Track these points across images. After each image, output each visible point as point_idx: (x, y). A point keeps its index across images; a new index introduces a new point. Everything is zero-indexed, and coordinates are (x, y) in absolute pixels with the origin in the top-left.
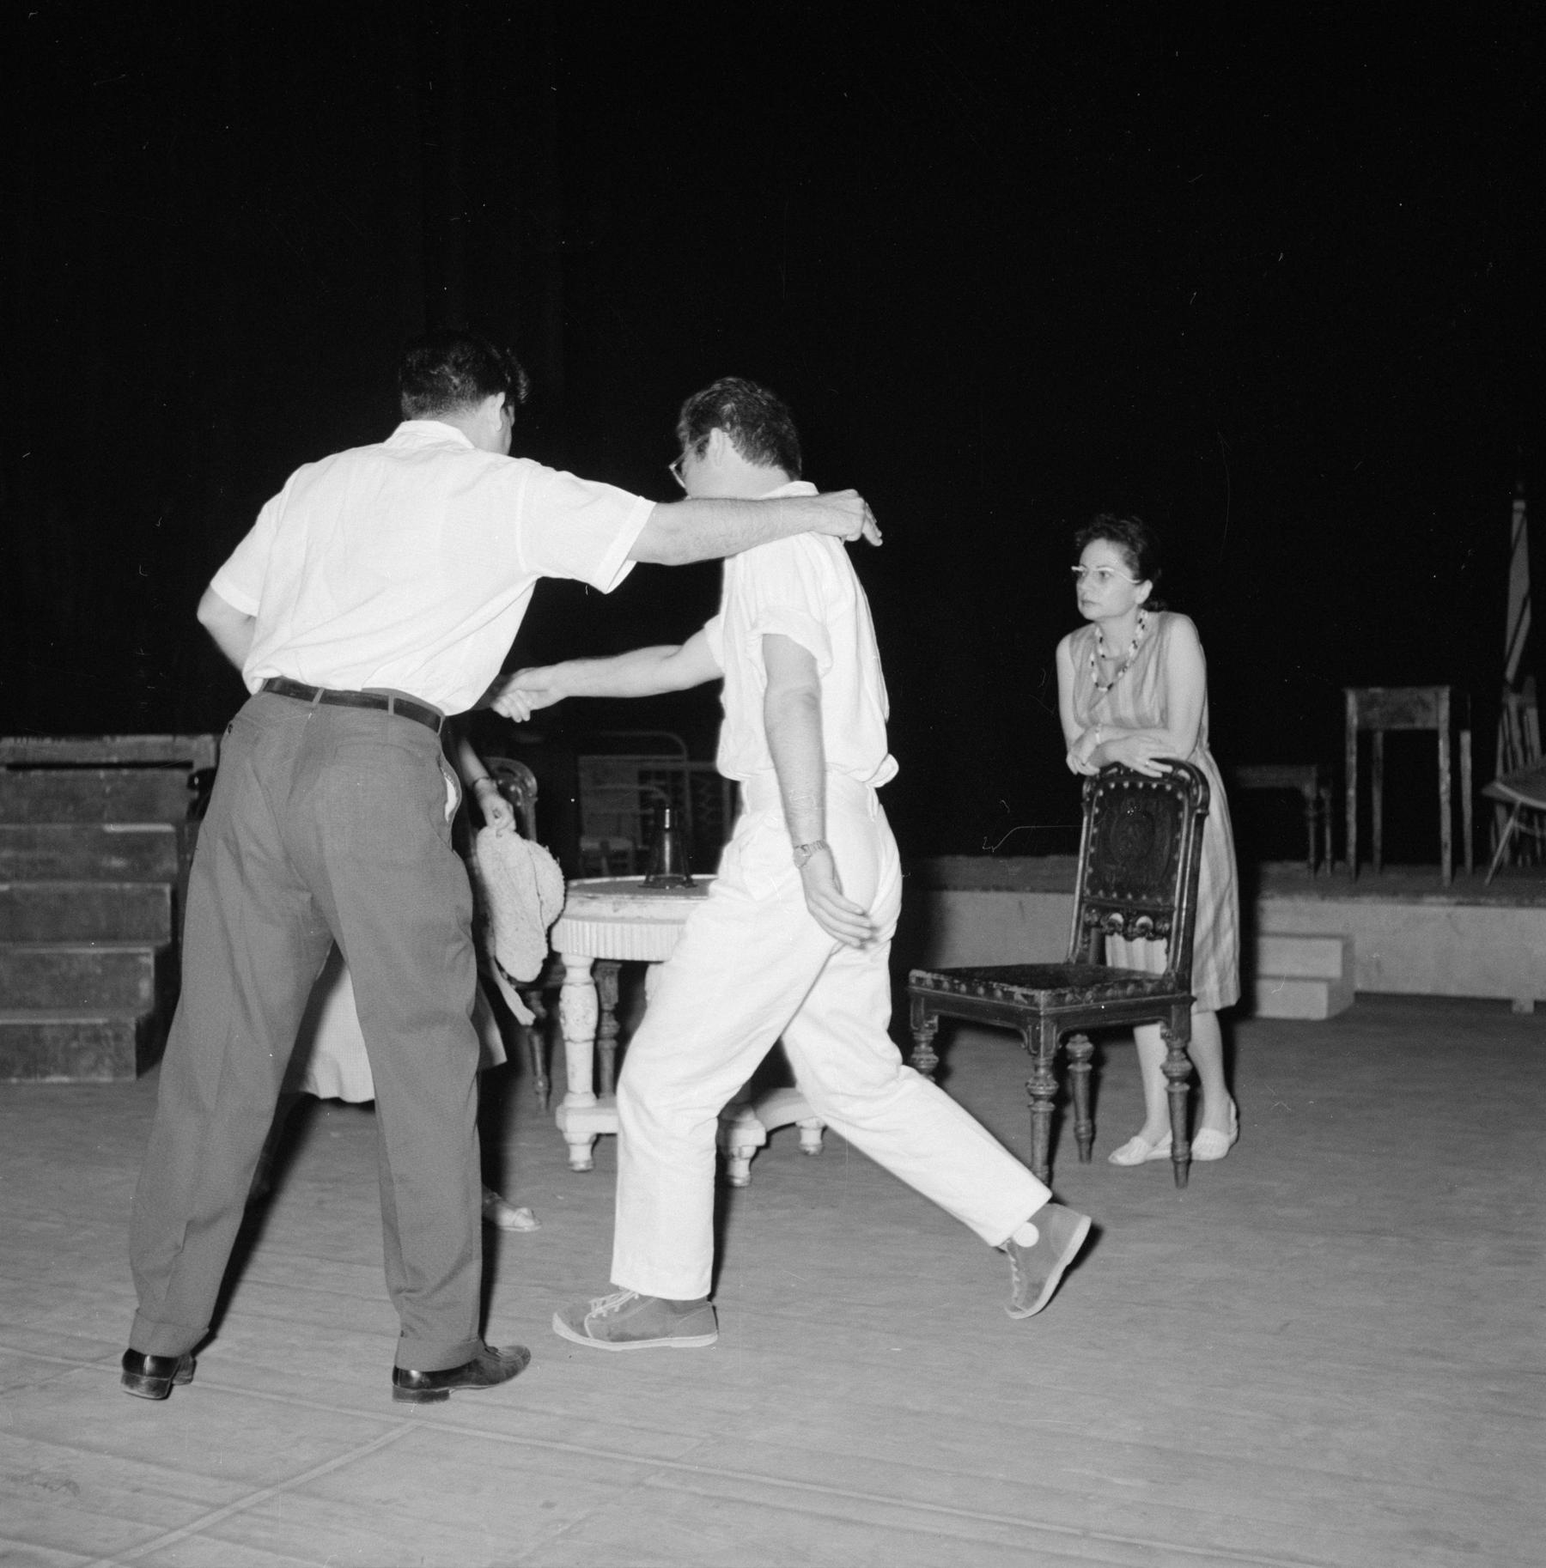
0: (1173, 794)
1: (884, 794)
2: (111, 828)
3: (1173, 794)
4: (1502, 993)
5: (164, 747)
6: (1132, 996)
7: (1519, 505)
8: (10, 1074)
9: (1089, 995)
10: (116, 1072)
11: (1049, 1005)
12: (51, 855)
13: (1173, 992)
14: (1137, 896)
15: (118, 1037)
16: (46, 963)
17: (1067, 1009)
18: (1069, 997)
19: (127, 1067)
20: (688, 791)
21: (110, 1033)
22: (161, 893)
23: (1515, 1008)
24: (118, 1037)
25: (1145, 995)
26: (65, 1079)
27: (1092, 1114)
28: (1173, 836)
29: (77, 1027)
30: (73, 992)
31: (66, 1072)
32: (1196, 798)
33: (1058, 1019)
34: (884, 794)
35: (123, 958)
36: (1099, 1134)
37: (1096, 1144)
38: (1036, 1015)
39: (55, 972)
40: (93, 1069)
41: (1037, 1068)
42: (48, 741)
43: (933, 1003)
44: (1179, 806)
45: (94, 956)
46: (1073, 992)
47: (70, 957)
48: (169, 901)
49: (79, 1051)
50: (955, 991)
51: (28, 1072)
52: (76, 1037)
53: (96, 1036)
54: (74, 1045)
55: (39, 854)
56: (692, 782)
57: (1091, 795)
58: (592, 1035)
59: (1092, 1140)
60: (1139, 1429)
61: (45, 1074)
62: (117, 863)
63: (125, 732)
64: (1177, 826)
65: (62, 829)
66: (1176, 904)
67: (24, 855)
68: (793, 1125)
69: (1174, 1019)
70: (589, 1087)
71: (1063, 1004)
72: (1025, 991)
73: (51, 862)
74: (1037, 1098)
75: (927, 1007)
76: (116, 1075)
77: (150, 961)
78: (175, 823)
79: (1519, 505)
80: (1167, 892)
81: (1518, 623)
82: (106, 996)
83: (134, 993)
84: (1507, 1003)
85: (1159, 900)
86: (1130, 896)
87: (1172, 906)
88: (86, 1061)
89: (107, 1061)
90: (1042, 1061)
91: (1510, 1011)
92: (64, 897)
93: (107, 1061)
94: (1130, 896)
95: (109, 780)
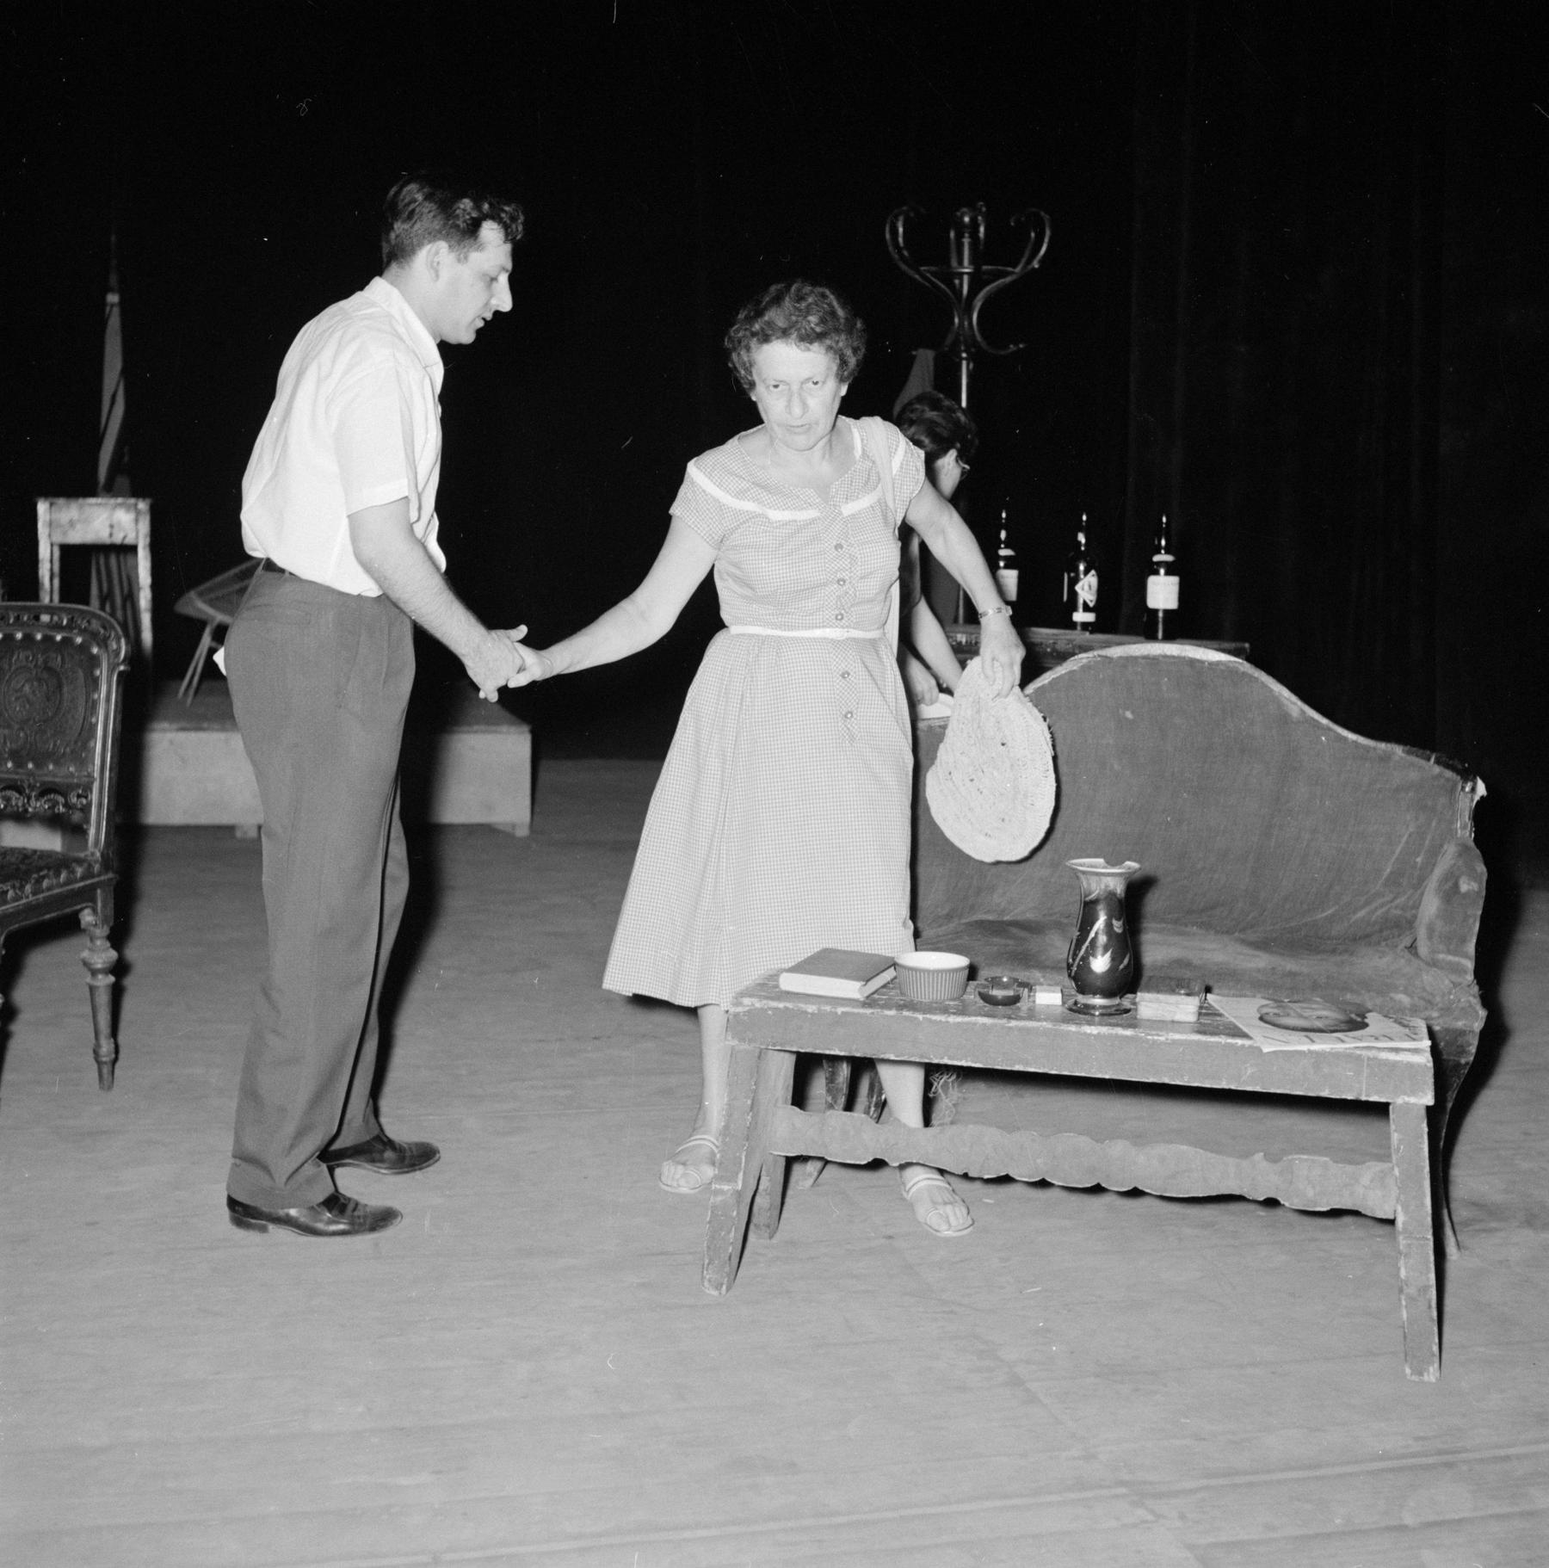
0: (84, 648)
3: (84, 648)
4: (224, 819)
6: (66, 884)
7: (113, 298)
9: (28, 888)
18: (11, 894)
23: (239, 834)
25: (76, 881)
27: (114, 1032)
28: (88, 695)
32: (117, 653)
36: (122, 1055)
37: (118, 1065)
44: (94, 662)
46: (14, 887)
59: (116, 1060)
60: (360, 1409)
64: (95, 683)
66: (96, 775)
69: (99, 904)
79: (113, 298)
81: (114, 419)
84: (230, 829)
86: (30, 766)
87: (90, 776)
91: (233, 837)
94: (30, 766)
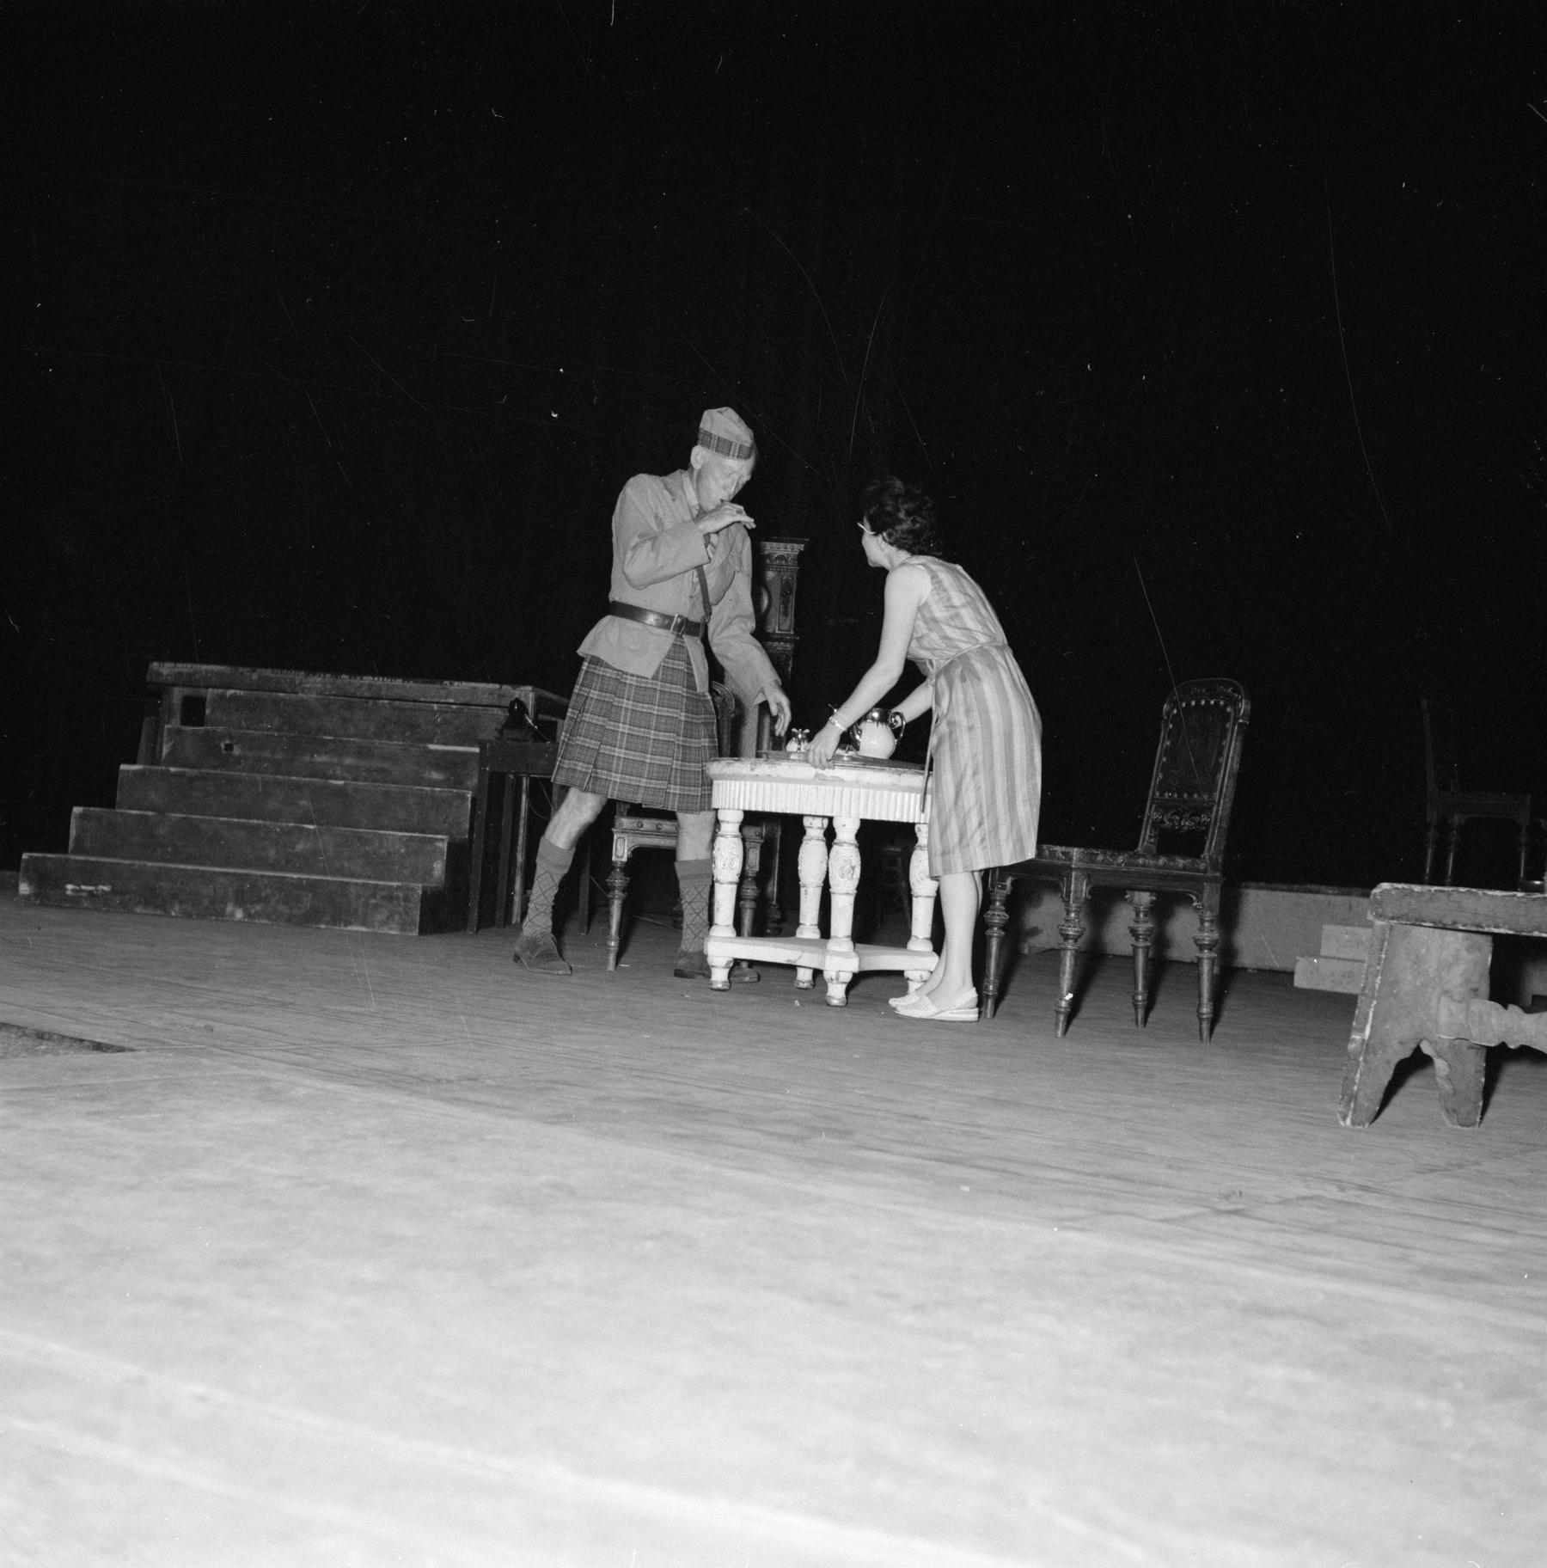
2: (432, 747)
5: (491, 693)
6: (1164, 867)
8: (319, 922)
9: (1120, 859)
10: (404, 927)
11: (1080, 860)
13: (1205, 871)
14: (1190, 795)
18: (1100, 858)
22: (463, 797)
24: (406, 899)
26: (363, 929)
30: (381, 864)
31: (364, 924)
33: (1089, 874)
40: (384, 923)
41: (1068, 913)
44: (1227, 717)
48: (469, 804)
49: (376, 906)
51: (335, 920)
52: (374, 896)
53: (390, 897)
54: (373, 901)
55: (375, 763)
57: (1168, 714)
58: (736, 879)
61: (348, 923)
62: (436, 776)
63: (460, 679)
65: (395, 745)
67: (363, 763)
68: (901, 973)
70: (730, 921)
71: (1094, 862)
72: (1064, 849)
73: (383, 770)
74: (1066, 937)
76: (403, 930)
77: (444, 846)
78: (483, 748)
80: (1210, 787)
82: (407, 872)
83: (429, 871)
85: (1206, 797)
89: (397, 917)
90: (1073, 906)
93: (397, 917)
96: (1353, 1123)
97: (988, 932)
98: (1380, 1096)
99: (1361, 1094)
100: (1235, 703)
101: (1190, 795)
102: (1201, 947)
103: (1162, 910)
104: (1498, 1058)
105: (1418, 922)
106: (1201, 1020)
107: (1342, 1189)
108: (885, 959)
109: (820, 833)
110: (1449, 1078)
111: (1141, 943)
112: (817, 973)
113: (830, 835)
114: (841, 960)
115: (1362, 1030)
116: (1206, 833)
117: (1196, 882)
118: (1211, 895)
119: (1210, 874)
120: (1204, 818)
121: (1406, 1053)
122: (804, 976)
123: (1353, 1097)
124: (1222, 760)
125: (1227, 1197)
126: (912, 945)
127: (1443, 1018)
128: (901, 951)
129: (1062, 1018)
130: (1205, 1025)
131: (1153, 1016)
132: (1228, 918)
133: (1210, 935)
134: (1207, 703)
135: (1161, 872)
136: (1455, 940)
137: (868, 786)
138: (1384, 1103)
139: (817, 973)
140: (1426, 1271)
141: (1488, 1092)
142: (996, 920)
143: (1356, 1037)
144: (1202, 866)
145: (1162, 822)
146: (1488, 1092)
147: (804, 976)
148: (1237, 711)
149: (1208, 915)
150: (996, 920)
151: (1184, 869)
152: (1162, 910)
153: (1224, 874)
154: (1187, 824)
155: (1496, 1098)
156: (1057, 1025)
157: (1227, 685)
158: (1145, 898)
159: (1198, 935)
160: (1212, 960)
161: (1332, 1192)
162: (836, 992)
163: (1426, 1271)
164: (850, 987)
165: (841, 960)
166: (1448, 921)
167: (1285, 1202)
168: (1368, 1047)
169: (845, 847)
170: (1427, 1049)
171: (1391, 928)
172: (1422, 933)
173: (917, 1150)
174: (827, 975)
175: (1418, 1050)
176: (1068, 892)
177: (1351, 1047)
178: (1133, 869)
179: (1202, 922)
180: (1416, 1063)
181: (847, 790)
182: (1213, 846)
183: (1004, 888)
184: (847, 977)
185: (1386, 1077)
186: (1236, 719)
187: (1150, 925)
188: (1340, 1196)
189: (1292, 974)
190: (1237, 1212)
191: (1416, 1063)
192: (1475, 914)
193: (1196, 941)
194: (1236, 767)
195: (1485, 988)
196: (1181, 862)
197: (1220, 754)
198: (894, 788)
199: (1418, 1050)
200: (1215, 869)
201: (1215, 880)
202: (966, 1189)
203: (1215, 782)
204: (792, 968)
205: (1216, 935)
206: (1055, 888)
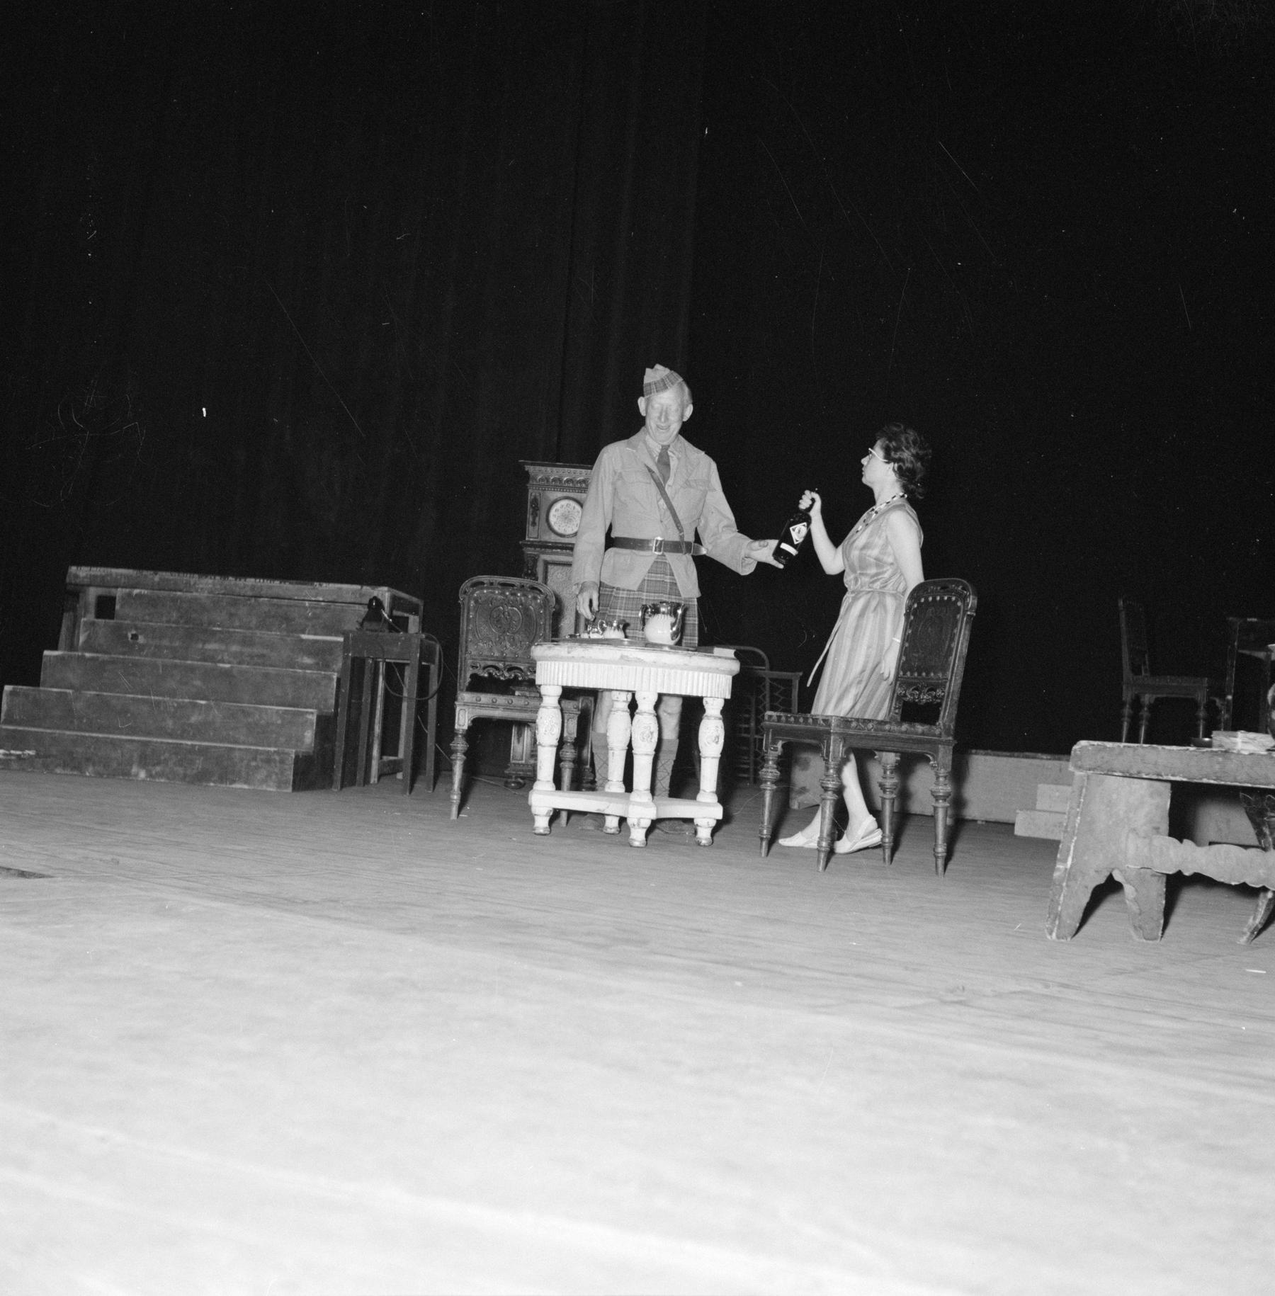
1: (1180, 872)
2: (304, 636)
8: (209, 781)
10: (280, 784)
12: (265, 652)
14: (928, 674)
15: (282, 762)
16: (246, 713)
17: (851, 732)
19: (286, 782)
20: (767, 692)
21: (277, 758)
22: (330, 679)
26: (246, 787)
29: (257, 751)
30: (261, 732)
34: (1180, 872)
35: (295, 714)
38: (829, 733)
39: (250, 720)
40: (264, 781)
42: (277, 583)
43: (778, 733)
45: (277, 711)
47: (261, 711)
49: (257, 768)
50: (787, 722)
51: (222, 779)
52: (255, 759)
54: (253, 764)
55: (257, 650)
56: (771, 686)
58: (555, 742)
61: (233, 782)
62: (308, 660)
65: (274, 635)
67: (247, 650)
69: (940, 755)
71: (849, 727)
73: (263, 656)
74: (826, 789)
75: (774, 735)
76: (279, 787)
77: (314, 718)
82: (282, 739)
88: (261, 775)
92: (266, 675)
95: (312, 608)
96: (1058, 937)
97: (763, 786)
98: (1080, 915)
99: (1064, 914)
100: (964, 599)
101: (928, 674)
102: (937, 798)
103: (906, 767)
104: (1176, 884)
105: (1110, 772)
106: (937, 858)
107: (1047, 987)
108: (680, 809)
109: (625, 706)
110: (1136, 900)
111: (888, 795)
112: (622, 820)
113: (633, 707)
114: (642, 809)
115: (1065, 861)
116: (940, 705)
117: (934, 744)
118: (945, 756)
119: (944, 738)
120: (939, 692)
121: (1101, 880)
122: (612, 823)
123: (1058, 916)
124: (954, 645)
125: (952, 992)
126: (700, 797)
127: (1131, 851)
128: (692, 802)
129: (822, 855)
130: (940, 862)
131: (897, 855)
132: (958, 774)
133: (945, 788)
134: (942, 598)
135: (904, 736)
136: (1141, 787)
137: (664, 666)
138: (1083, 921)
139: (622, 820)
140: (1111, 1047)
141: (1168, 912)
142: (769, 776)
143: (1060, 866)
144: (937, 732)
145: (905, 696)
146: (1168, 912)
147: (612, 823)
148: (965, 604)
149: (942, 772)
150: (769, 776)
151: (923, 734)
152: (906, 767)
153: (955, 738)
154: (925, 698)
155: (1174, 919)
156: (818, 861)
157: (958, 584)
158: (891, 758)
159: (933, 787)
160: (946, 809)
161: (1039, 988)
162: (638, 836)
163: (1111, 1047)
164: (649, 831)
165: (642, 809)
166: (1134, 771)
167: (999, 995)
168: (1070, 875)
169: (646, 716)
170: (1118, 877)
171: (1088, 777)
172: (1112, 782)
173: (705, 956)
174: (630, 822)
175: (1110, 878)
176: (828, 752)
177: (1056, 874)
178: (880, 734)
179: (938, 778)
180: (1109, 888)
181: (647, 669)
182: (947, 716)
183: (776, 750)
184: (647, 823)
185: (1085, 899)
186: (965, 611)
187: (895, 780)
188: (1045, 991)
189: (1013, 825)
190: (960, 1003)
191: (1109, 888)
192: (1156, 764)
193: (932, 793)
194: (965, 651)
195: (1165, 826)
196: (920, 728)
197: (952, 640)
198: (685, 667)
199: (1110, 878)
200: (948, 734)
201: (947, 743)
202: (739, 984)
203: (947, 662)
204: (600, 817)
205: (949, 788)
206: (816, 749)
